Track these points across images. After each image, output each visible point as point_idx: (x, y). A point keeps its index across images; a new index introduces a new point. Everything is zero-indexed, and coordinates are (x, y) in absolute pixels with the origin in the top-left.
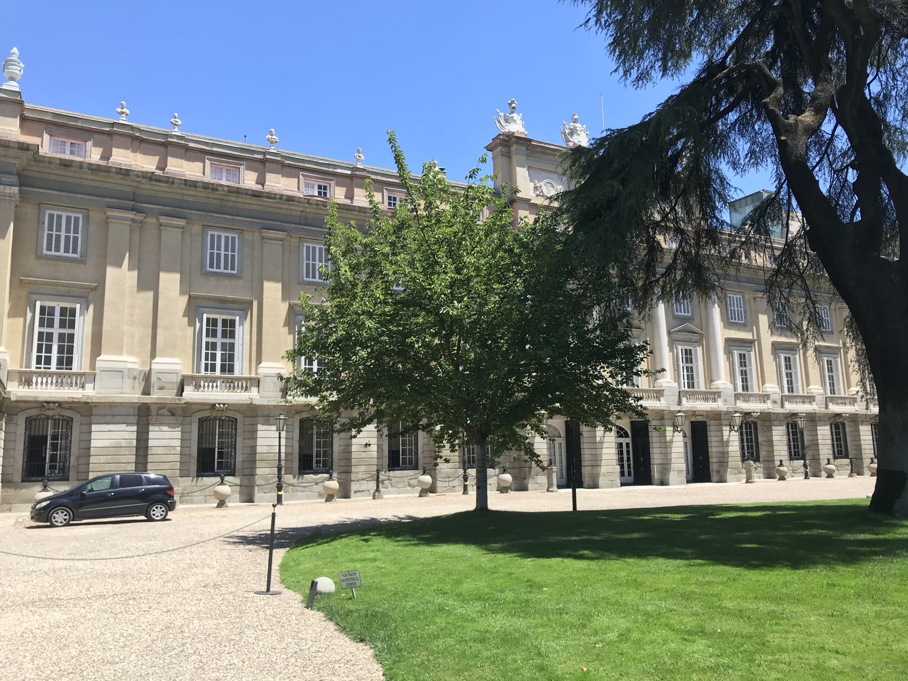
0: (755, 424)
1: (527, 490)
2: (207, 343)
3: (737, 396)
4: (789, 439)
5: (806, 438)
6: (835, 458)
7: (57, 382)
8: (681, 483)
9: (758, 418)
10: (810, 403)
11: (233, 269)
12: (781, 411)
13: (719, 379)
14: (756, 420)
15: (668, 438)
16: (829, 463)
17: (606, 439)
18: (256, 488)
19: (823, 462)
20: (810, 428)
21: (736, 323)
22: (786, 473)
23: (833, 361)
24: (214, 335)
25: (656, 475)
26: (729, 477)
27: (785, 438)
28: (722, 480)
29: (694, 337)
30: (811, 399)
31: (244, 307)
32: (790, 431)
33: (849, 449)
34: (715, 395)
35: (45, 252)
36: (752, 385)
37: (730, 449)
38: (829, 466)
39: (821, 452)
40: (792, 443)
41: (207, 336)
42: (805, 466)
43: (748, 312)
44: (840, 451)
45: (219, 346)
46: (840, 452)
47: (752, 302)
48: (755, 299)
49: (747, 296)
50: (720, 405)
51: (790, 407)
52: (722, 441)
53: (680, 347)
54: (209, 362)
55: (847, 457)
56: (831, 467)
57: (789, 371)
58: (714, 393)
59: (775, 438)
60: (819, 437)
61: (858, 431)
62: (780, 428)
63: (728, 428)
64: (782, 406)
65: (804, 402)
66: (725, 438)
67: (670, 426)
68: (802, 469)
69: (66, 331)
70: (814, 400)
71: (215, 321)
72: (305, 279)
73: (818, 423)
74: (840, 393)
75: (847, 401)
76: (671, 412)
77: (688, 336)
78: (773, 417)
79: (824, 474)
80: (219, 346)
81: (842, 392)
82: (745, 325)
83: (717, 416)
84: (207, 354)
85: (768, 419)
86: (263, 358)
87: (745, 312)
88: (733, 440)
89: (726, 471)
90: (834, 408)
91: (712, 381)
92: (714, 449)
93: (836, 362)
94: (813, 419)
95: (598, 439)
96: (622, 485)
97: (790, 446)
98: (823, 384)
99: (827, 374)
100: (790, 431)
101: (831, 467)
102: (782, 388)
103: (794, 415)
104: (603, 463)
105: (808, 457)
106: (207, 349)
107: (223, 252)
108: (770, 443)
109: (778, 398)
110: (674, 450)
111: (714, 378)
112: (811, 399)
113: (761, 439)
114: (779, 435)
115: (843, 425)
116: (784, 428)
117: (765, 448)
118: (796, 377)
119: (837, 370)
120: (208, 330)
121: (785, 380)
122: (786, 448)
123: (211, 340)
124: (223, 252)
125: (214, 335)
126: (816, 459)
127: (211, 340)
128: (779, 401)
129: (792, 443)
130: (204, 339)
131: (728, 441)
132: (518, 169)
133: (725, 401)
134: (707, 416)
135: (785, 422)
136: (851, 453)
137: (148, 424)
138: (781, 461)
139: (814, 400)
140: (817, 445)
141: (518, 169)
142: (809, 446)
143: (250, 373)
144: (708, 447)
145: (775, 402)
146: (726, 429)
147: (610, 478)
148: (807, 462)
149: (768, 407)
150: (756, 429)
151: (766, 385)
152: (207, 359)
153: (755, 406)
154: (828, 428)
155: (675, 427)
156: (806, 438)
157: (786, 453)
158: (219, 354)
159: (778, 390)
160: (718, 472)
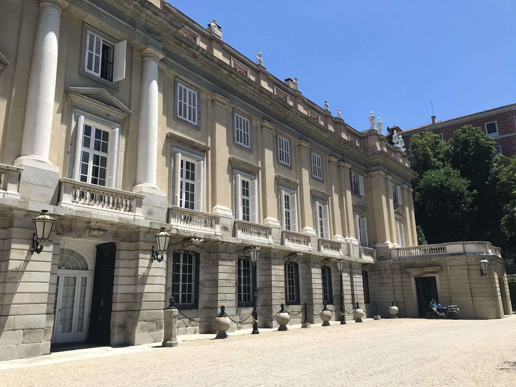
0: (197, 255)
1: (132, 345)
3: (170, 213)
4: (239, 279)
5: (259, 278)
6: (288, 304)
7: (113, 202)
9: (201, 246)
10: (266, 236)
11: (248, 145)
12: (232, 240)
13: (146, 179)
14: (198, 250)
16: (282, 311)
17: (152, 272)
18: (140, 324)
19: (276, 309)
20: (264, 267)
21: (186, 122)
22: (227, 326)
23: (290, 196)
26: (138, 335)
27: (234, 277)
28: (127, 342)
29: (114, 113)
30: (266, 231)
31: (203, 151)
32: (242, 268)
33: (301, 294)
34: (134, 201)
36: (199, 203)
37: (147, 288)
38: (282, 314)
39: (274, 296)
40: (242, 285)
42: (255, 315)
43: (203, 115)
44: (294, 295)
46: (292, 297)
47: (210, 104)
48: (213, 101)
49: (203, 96)
50: (138, 217)
51: (242, 237)
52: (136, 275)
53: (83, 121)
55: (298, 303)
56: (285, 315)
57: (246, 198)
58: (131, 198)
59: (221, 276)
60: (273, 278)
61: (310, 273)
62: (230, 263)
63: (149, 256)
64: (234, 235)
65: (259, 234)
66: (141, 271)
67: (22, 240)
68: (251, 319)
70: (270, 233)
72: (86, 70)
73: (274, 261)
74: (295, 230)
75: (302, 240)
76: (29, 213)
77: (103, 109)
78: (221, 247)
79: (276, 325)
81: (296, 228)
82: (197, 128)
83: (132, 235)
85: (213, 249)
86: (218, 199)
87: (199, 113)
88: (156, 277)
89: (135, 324)
90: (291, 245)
91: (135, 184)
92: (121, 288)
93: (293, 198)
94: (267, 254)
97: (239, 289)
98: (280, 218)
99: (284, 210)
100: (242, 268)
101: (285, 315)
102: (236, 215)
103: (248, 248)
105: (259, 303)
108: (214, 282)
109: (229, 223)
111: (139, 178)
112: (266, 231)
113: (202, 277)
114: (226, 272)
115: (297, 265)
116: (234, 263)
117: (207, 290)
118: (254, 206)
119: (294, 207)
121: (319, 226)
122: (234, 290)
126: (268, 305)
128: (230, 228)
129: (242, 285)
131: (145, 277)
133: (150, 213)
134: (116, 234)
135: (236, 256)
136: (303, 297)
137: (271, 264)
138: (223, 308)
139: (270, 233)
140: (270, 287)
142: (262, 289)
143: (208, 211)
144: (112, 285)
145: (225, 228)
146: (144, 261)
148: (258, 308)
149: (216, 232)
150: (198, 262)
151: (218, 206)
153: (197, 230)
154: (282, 267)
155: (154, 255)
156: (259, 278)
157: (233, 297)
159: (230, 214)
160: (123, 327)
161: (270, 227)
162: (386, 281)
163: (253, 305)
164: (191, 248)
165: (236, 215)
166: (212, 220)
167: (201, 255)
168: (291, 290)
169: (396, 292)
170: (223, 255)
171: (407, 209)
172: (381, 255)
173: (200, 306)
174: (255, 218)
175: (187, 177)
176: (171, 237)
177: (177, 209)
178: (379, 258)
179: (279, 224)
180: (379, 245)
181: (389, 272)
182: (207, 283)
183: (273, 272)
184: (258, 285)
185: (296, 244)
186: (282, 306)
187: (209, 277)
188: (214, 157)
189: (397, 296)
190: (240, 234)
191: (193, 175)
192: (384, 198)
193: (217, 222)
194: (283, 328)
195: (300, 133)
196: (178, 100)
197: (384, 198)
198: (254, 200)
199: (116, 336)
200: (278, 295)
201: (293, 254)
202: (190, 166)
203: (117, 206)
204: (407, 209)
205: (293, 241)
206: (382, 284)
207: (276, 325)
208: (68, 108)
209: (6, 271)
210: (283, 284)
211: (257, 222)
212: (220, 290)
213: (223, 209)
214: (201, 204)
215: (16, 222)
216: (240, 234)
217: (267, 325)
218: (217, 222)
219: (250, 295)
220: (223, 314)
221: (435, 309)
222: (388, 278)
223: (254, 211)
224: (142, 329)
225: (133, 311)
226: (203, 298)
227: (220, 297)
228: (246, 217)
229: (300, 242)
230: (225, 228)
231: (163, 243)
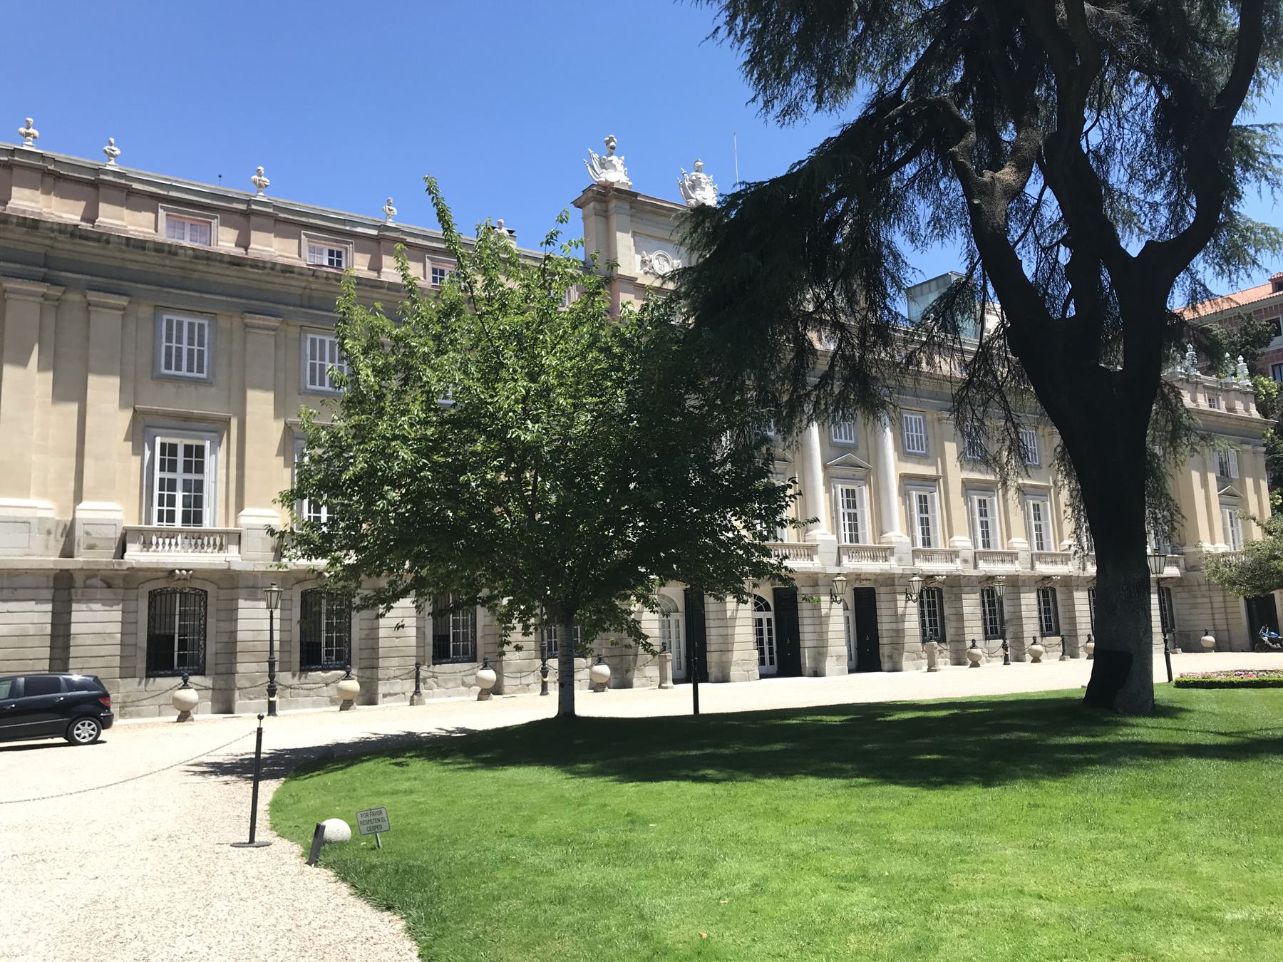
0: (940, 591)
1: (822, 675)
2: (162, 480)
3: (916, 554)
6: (1043, 636)
8: (842, 673)
9: (944, 582)
11: (200, 370)
13: (891, 529)
15: (824, 612)
16: (1035, 643)
19: (1028, 641)
20: (1011, 596)
24: (173, 468)
25: (807, 662)
27: (979, 610)
28: (896, 669)
29: (859, 473)
30: (1012, 556)
34: (885, 552)
35: (164, 371)
36: (936, 538)
37: (907, 625)
38: (1035, 647)
39: (1025, 628)
41: (162, 469)
42: (1005, 647)
45: (179, 485)
46: (1049, 628)
47: (936, 424)
49: (929, 417)
50: (892, 566)
51: (985, 568)
52: (896, 614)
53: (839, 487)
54: (165, 508)
55: (1057, 634)
56: (1038, 647)
58: (885, 549)
59: (966, 610)
60: (1023, 608)
61: (1072, 599)
62: (973, 596)
64: (976, 567)
65: (1003, 561)
66: (900, 611)
67: (825, 594)
68: (1001, 652)
69: (193, 477)
71: (173, 449)
72: (309, 386)
73: (1022, 589)
75: (1059, 559)
76: (827, 575)
78: (963, 582)
79: (1028, 657)
80: (179, 485)
82: (926, 456)
83: (889, 580)
84: (161, 497)
85: (956, 584)
90: (1043, 569)
91: (882, 533)
92: (885, 625)
94: (1015, 583)
95: (729, 614)
96: (762, 676)
98: (1028, 536)
101: (1038, 647)
104: (736, 646)
105: (1008, 635)
106: (161, 488)
107: (185, 347)
108: (960, 617)
109: (969, 555)
110: (831, 628)
112: (1012, 556)
115: (1054, 590)
116: (978, 596)
117: (953, 624)
118: (935, 525)
120: (162, 461)
122: (980, 623)
123: (167, 475)
124: (185, 347)
125: (173, 468)
126: (1019, 638)
127: (167, 475)
128: (971, 560)
130: (158, 475)
131: (904, 615)
132: (619, 234)
134: (876, 581)
135: (979, 589)
136: (1064, 628)
138: (973, 641)
141: (619, 234)
142: (1011, 620)
144: (704, 619)
145: (965, 561)
146: (901, 599)
147: (746, 668)
149: (956, 567)
150: (941, 598)
152: (161, 504)
153: (939, 567)
154: (1034, 595)
156: (1007, 609)
158: (179, 496)
160: (891, 657)
161: (957, 549)
162: (1199, 600)
163: (1003, 637)
164: (933, 585)
165: (913, 543)
166: (952, 555)
167: (944, 590)
168: (1048, 619)
169: (1217, 616)
170: (966, 589)
171: (1249, 482)
172: (1191, 563)
173: (948, 639)
174: (998, 545)
175: (849, 507)
176: (330, 551)
177: (919, 550)
178: (1190, 568)
179: (1026, 546)
180: (1187, 550)
181: (1204, 588)
182: (952, 618)
183: (1023, 601)
184: (1006, 618)
185: (1050, 566)
186: (1034, 638)
187: (953, 611)
188: (946, 484)
189: (1217, 622)
190: (981, 564)
191: (854, 502)
192: (1196, 476)
193: (957, 556)
194: (1036, 660)
195: (241, 297)
196: (164, 344)
197: (1196, 476)
198: (994, 520)
199: (886, 663)
200: (1031, 626)
201: (1048, 578)
202: (850, 494)
203: (875, 558)
204: (1249, 482)
205: (1046, 563)
206: (1194, 606)
207: (1028, 657)
208: (829, 480)
209: (53, 601)
210: (1036, 614)
211: (1000, 549)
212: (966, 624)
213: (962, 541)
214: (939, 543)
215: (820, 582)
216: (981, 564)
217: (1019, 659)
218: (957, 556)
219: (996, 626)
220: (974, 646)
221: (1266, 639)
222: (1203, 596)
223: (995, 534)
224: (907, 659)
225: (898, 644)
226: (950, 632)
227: (966, 631)
228: (987, 544)
229: (1056, 563)
230: (965, 561)
231: (917, 587)
